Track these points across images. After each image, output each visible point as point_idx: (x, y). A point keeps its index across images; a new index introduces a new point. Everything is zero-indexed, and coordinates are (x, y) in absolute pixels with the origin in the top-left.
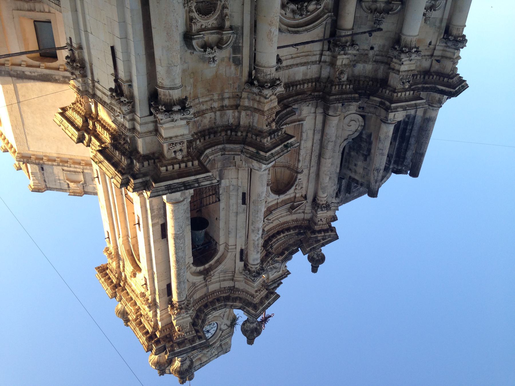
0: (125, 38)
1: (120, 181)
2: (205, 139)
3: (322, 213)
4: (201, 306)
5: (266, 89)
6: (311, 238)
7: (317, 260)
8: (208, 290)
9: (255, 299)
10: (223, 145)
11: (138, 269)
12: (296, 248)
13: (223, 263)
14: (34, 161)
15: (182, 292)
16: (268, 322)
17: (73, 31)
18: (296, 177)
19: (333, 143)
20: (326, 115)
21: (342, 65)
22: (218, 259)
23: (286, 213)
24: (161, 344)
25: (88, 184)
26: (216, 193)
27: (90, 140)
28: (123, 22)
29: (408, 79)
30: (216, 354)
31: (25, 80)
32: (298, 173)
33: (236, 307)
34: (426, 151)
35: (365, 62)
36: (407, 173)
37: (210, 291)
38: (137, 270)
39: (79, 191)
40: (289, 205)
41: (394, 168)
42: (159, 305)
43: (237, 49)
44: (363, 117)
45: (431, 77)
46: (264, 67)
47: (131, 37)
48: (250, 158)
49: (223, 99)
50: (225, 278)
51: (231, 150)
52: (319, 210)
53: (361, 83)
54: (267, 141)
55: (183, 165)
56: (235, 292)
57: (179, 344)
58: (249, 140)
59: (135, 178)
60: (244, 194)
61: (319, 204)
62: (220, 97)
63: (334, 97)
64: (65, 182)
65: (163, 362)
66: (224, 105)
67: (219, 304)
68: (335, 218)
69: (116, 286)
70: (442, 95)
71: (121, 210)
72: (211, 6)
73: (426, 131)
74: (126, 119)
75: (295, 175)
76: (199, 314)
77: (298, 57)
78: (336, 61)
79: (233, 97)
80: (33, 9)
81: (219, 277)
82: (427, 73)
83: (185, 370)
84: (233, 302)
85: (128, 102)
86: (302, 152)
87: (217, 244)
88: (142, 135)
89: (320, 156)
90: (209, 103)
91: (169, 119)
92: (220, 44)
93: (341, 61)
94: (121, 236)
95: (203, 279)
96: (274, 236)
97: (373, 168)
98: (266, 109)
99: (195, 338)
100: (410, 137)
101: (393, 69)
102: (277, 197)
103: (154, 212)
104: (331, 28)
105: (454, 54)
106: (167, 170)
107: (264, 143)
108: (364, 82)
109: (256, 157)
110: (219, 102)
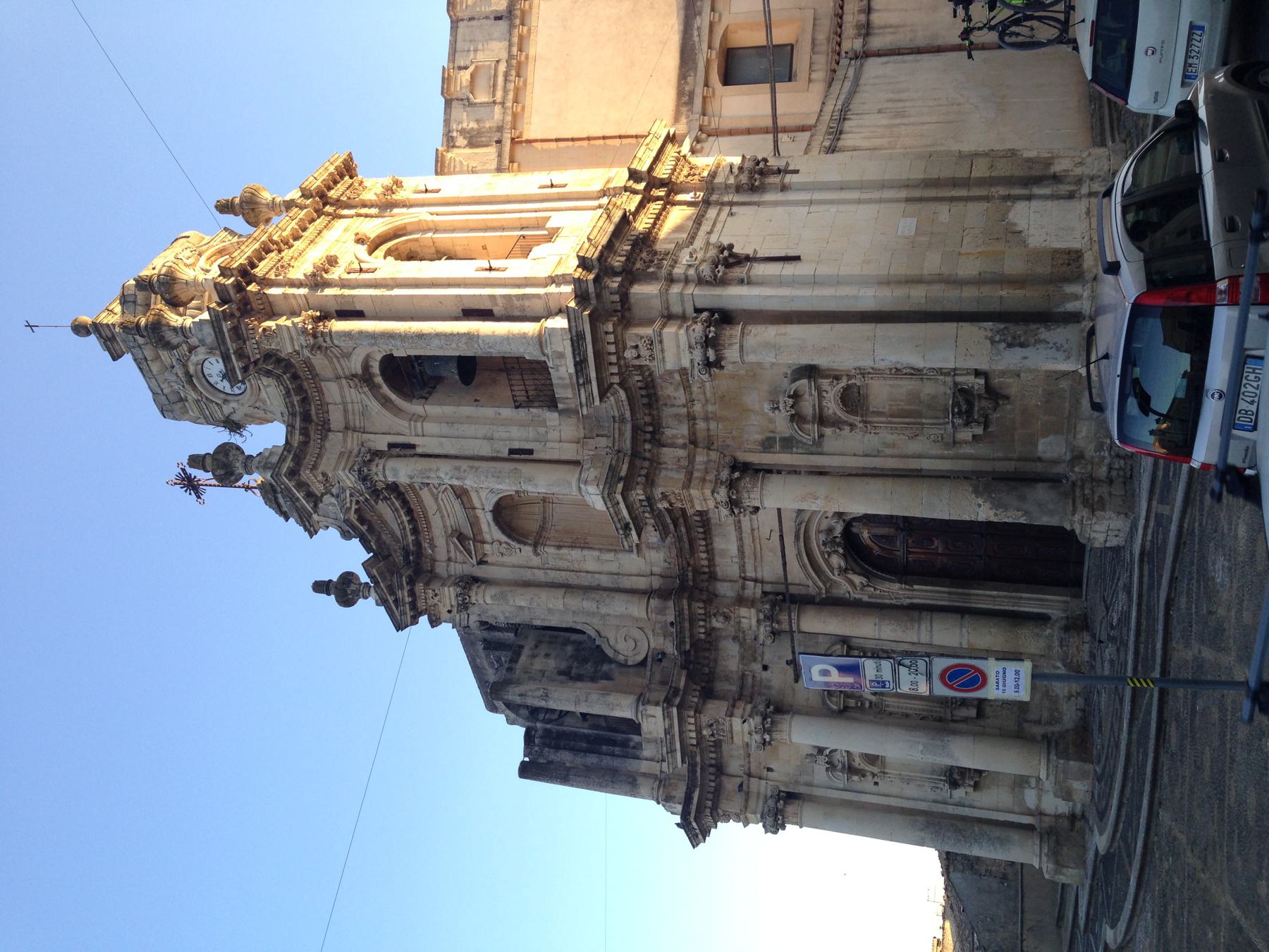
0: (815, 281)
1: (589, 255)
2: (640, 388)
3: (450, 595)
4: (295, 367)
5: (728, 492)
6: (401, 577)
7: (346, 591)
8: (325, 381)
9: (308, 472)
10: (629, 419)
11: (373, 247)
12: (374, 547)
13: (384, 411)
14: (519, 7)
15: (351, 339)
16: (186, 491)
17: (811, 179)
18: (525, 544)
19: (595, 610)
20: (649, 593)
21: (739, 617)
22: (391, 400)
23: (449, 525)
24: (235, 294)
25: (468, 109)
26: (529, 401)
27: (635, 192)
28: (838, 281)
29: (717, 734)
30: (165, 391)
31: (682, 12)
32: (535, 545)
33: (291, 436)
34: (572, 786)
35: (742, 658)
36: (525, 756)
37: (322, 383)
38: (369, 246)
39: (452, 89)
40: (467, 531)
41: (536, 731)
42: (319, 293)
43: (788, 444)
44: (643, 663)
45: (713, 778)
46: (762, 489)
47: (819, 292)
48: (610, 465)
49: (707, 419)
50: (350, 413)
51: (621, 434)
52: (459, 589)
53: (707, 654)
54: (638, 494)
55: (613, 359)
56: (319, 432)
57: (236, 330)
58: (638, 462)
59: (596, 280)
60: (530, 452)
61: (470, 589)
62: (710, 415)
63: (686, 607)
64: (472, 62)
65: (176, 289)
66: (697, 422)
67: (298, 401)
68: (434, 622)
69: (322, 196)
70: (683, 801)
71: (489, 224)
72: (852, 405)
73: (613, 782)
74: (687, 269)
75: (529, 542)
76: (283, 364)
77: (753, 541)
78: (745, 606)
79: (709, 436)
80: (817, 49)
81: (353, 403)
82: (720, 769)
83: (162, 336)
84: (301, 429)
85: (716, 276)
86: (576, 554)
87: (423, 400)
88: (664, 294)
89: (567, 587)
90: (701, 397)
91: (693, 342)
92: (797, 418)
93: (746, 615)
94: (436, 218)
95: (354, 373)
96: (405, 503)
97: (550, 688)
98: (694, 492)
99: (246, 360)
100: (600, 753)
101: (734, 706)
102: (489, 507)
103: (518, 300)
104: (800, 595)
105: (754, 813)
106: (607, 333)
107: (635, 489)
108: (708, 658)
109: (612, 475)
110: (703, 414)
